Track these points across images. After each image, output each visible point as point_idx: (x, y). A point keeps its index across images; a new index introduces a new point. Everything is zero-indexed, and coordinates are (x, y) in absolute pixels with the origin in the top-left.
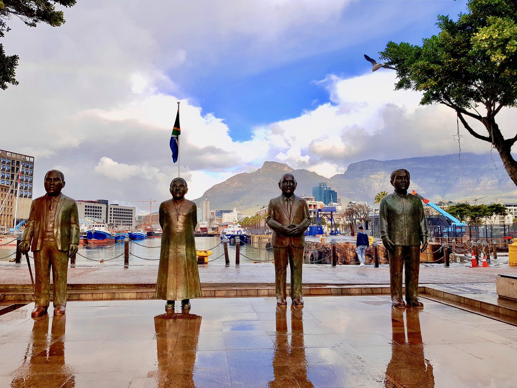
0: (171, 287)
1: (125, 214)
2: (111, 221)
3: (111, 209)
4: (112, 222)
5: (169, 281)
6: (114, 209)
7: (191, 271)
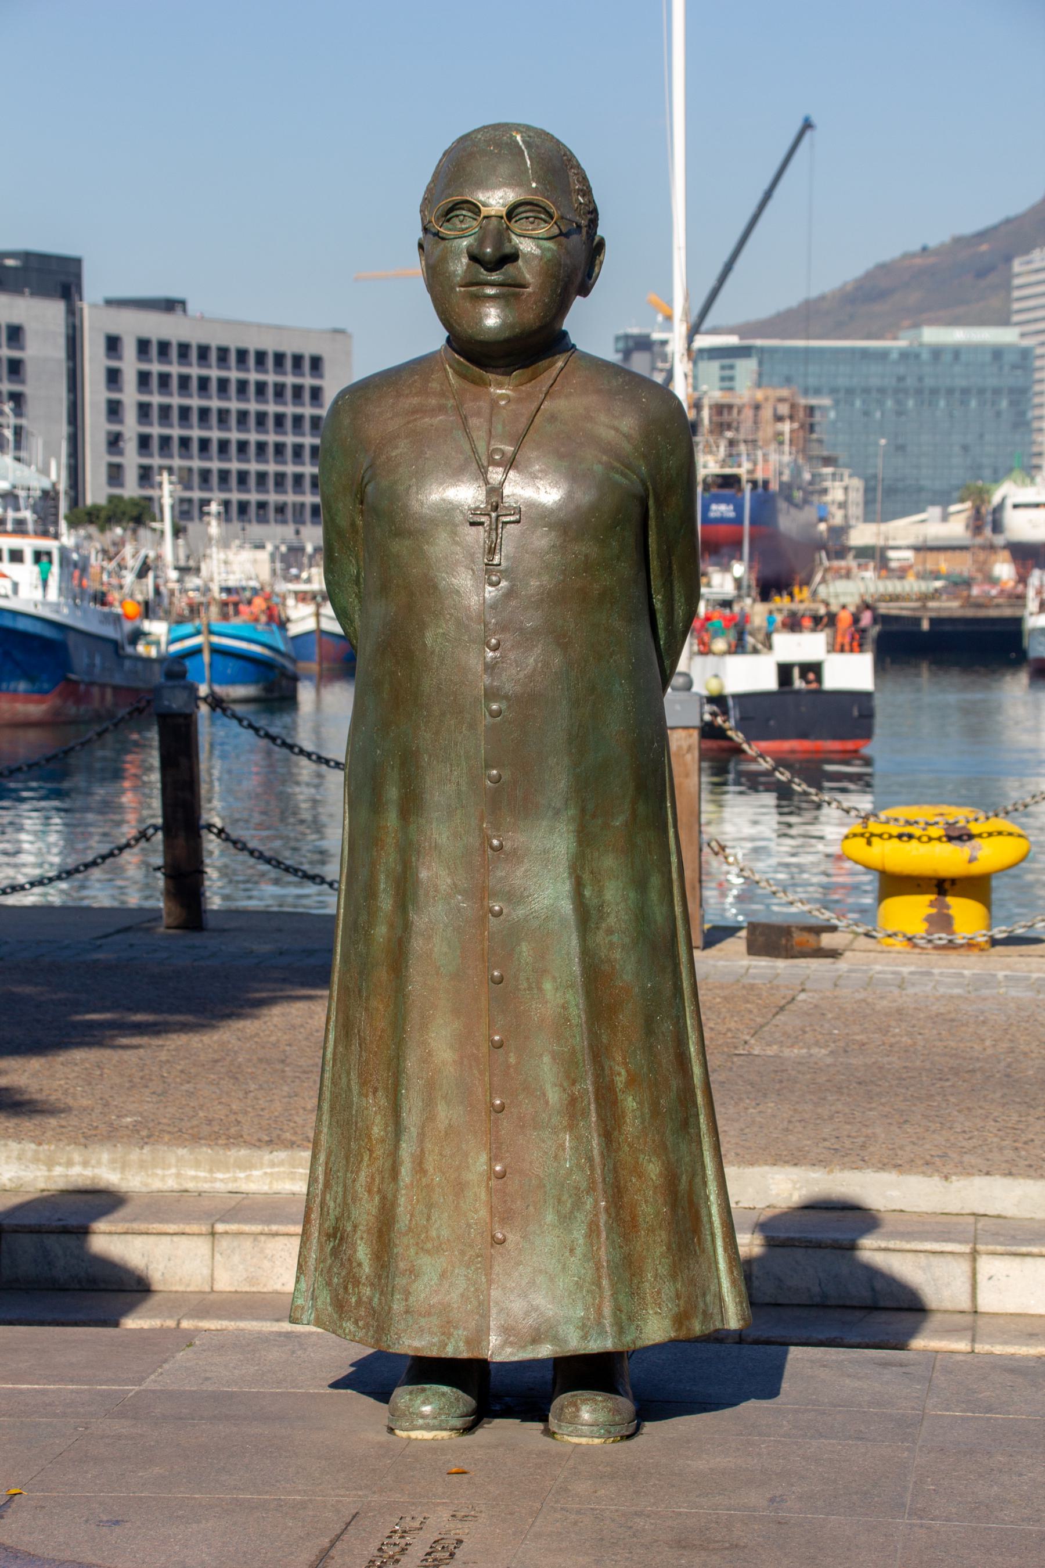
0: (441, 1227)
1: (289, 410)
2: (115, 473)
3: (113, 344)
4: (131, 489)
5: (420, 1167)
6: (143, 346)
7: (632, 1081)
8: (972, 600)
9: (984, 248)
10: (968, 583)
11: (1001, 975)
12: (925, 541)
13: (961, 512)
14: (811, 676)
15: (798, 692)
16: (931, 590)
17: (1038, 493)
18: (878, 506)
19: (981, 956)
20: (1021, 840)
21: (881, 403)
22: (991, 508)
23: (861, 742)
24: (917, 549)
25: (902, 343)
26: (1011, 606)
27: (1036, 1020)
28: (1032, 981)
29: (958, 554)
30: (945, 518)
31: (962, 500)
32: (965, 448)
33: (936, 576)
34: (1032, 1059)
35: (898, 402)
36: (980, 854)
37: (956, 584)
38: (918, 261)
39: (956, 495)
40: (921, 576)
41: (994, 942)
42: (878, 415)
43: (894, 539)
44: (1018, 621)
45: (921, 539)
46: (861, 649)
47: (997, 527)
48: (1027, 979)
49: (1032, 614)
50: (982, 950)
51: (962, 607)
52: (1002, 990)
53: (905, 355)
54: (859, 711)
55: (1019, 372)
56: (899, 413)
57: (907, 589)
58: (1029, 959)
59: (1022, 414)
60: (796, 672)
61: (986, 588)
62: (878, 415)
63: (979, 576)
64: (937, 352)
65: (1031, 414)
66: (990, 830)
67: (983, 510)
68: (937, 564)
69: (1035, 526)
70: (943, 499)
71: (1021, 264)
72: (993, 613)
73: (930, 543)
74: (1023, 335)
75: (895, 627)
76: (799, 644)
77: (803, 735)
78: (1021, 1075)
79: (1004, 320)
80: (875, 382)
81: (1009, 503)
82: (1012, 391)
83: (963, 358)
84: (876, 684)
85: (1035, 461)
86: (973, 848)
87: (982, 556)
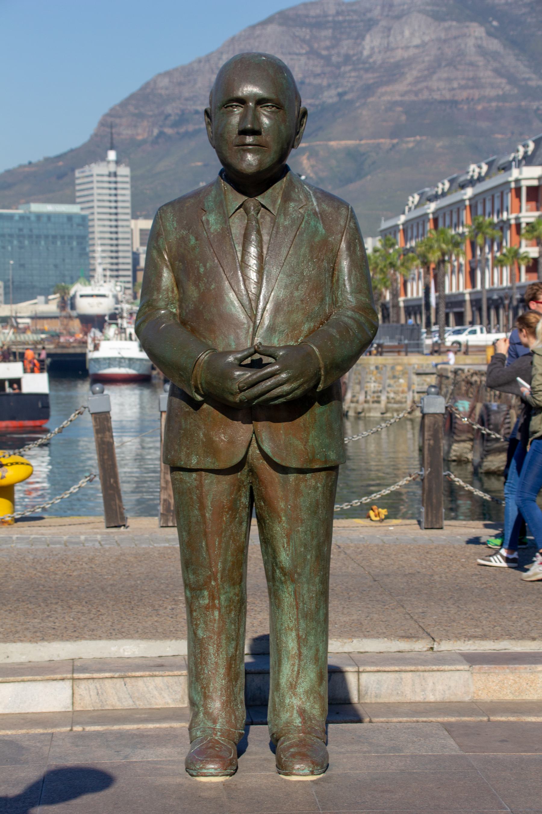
8: (60, 344)
9: (61, 164)
10: (58, 335)
11: (15, 537)
12: (36, 314)
13: (55, 297)
14: (15, 386)
15: (9, 395)
16: (39, 339)
17: (92, 290)
18: (11, 296)
19: (8, 528)
20: (28, 467)
21: (11, 242)
22: (69, 297)
23: (44, 421)
24: (32, 318)
25: (20, 211)
26: (81, 347)
27: (25, 560)
28: (30, 539)
29: (54, 321)
30: (47, 302)
31: (55, 293)
32: (56, 266)
33: (43, 332)
34: (15, 580)
35: (20, 242)
36: (7, 475)
37: (52, 336)
38: (27, 169)
39: (52, 290)
40: (35, 332)
41: (17, 520)
42: (9, 248)
43: (20, 313)
44: (84, 355)
45: (34, 313)
46: (41, 370)
47: (73, 307)
48: (28, 538)
49: (90, 351)
50: (10, 524)
51: (55, 348)
52: (13, 545)
53: (22, 218)
54: (42, 404)
55: (81, 228)
56: (21, 247)
57: (27, 338)
58: (33, 528)
59: (84, 249)
60: (7, 384)
61: (68, 338)
62: (9, 248)
63: (65, 332)
64: (39, 216)
65: (88, 249)
66: (12, 462)
67: (66, 298)
68: (43, 326)
69: (92, 307)
70: (46, 292)
71: (79, 173)
72: (71, 351)
73: (39, 315)
74: (82, 209)
75: (56, 359)
76: (8, 369)
77: (13, 418)
78: (6, 589)
79: (72, 201)
80: (7, 231)
81: (78, 295)
82: (78, 237)
83: (53, 219)
84: (50, 389)
85: (92, 273)
86: (3, 471)
87: (65, 321)
